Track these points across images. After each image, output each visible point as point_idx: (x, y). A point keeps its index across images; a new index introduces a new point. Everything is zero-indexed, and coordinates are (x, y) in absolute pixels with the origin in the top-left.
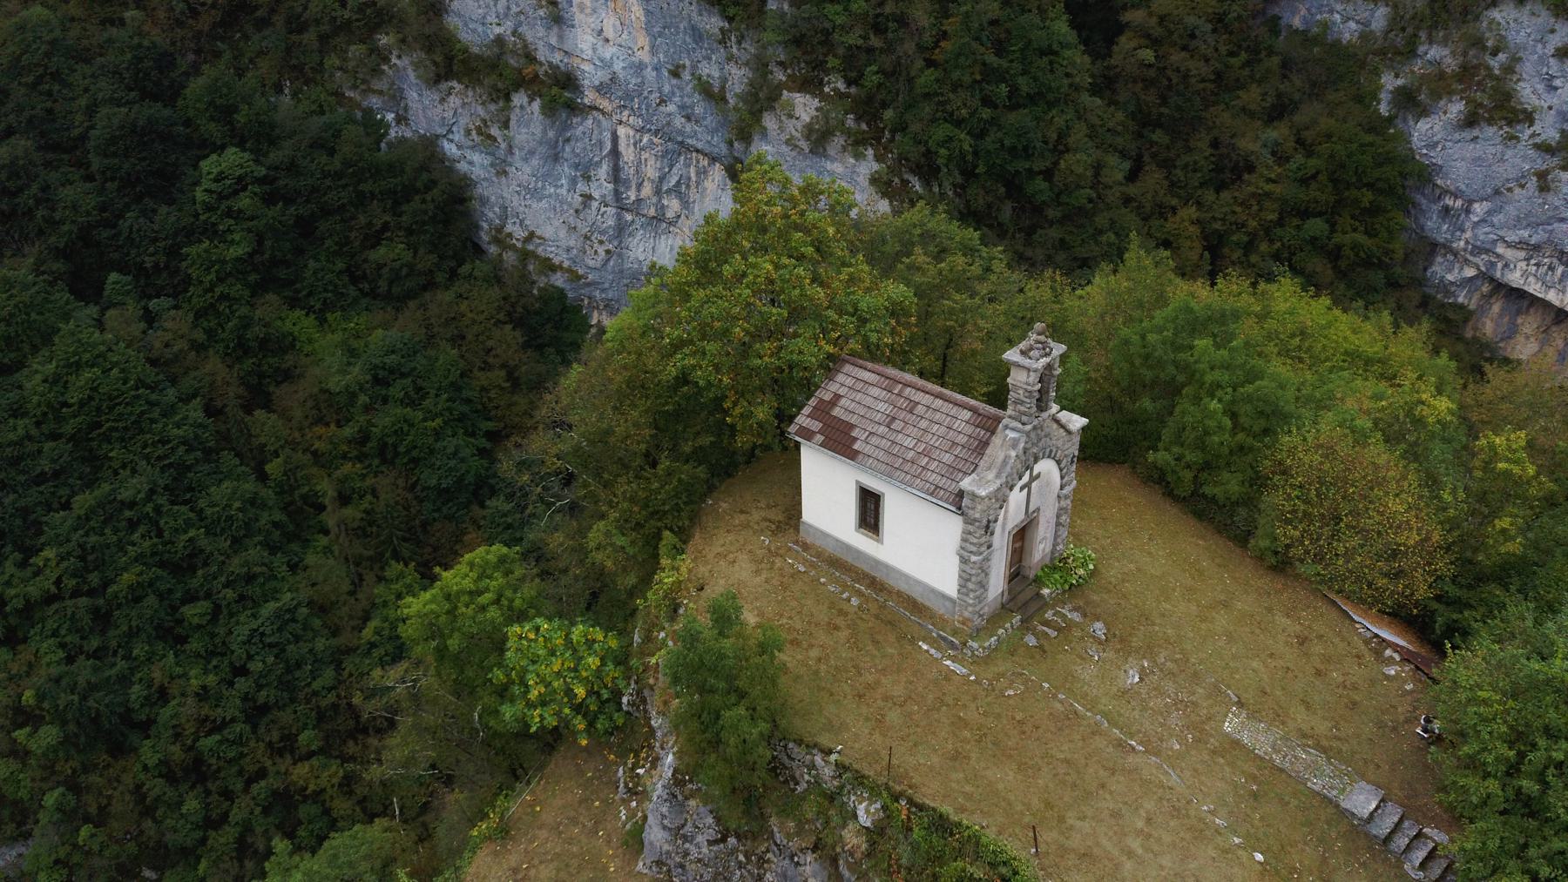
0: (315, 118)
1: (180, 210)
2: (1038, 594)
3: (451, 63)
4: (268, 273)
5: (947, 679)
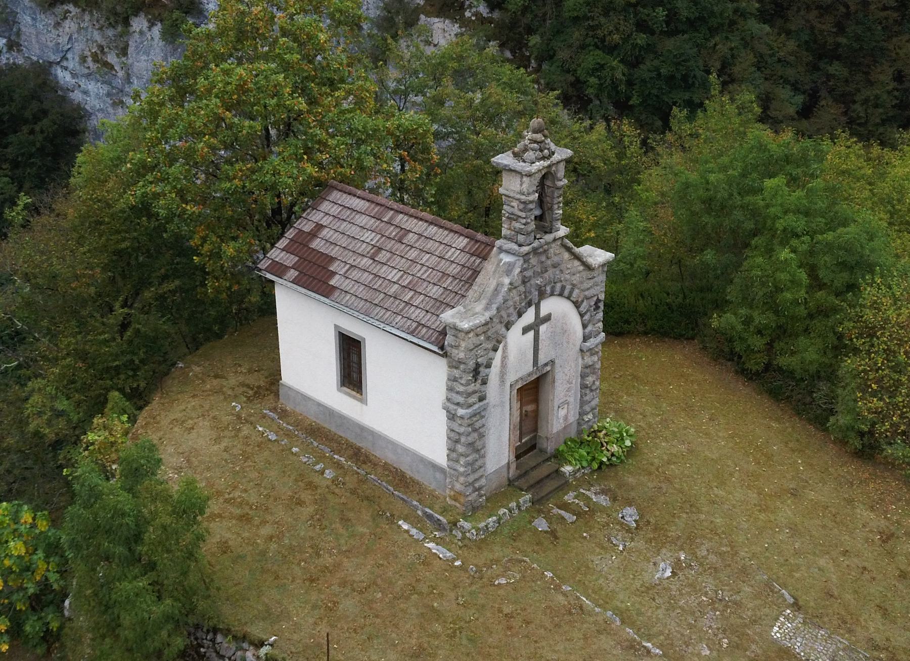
2: (557, 471)
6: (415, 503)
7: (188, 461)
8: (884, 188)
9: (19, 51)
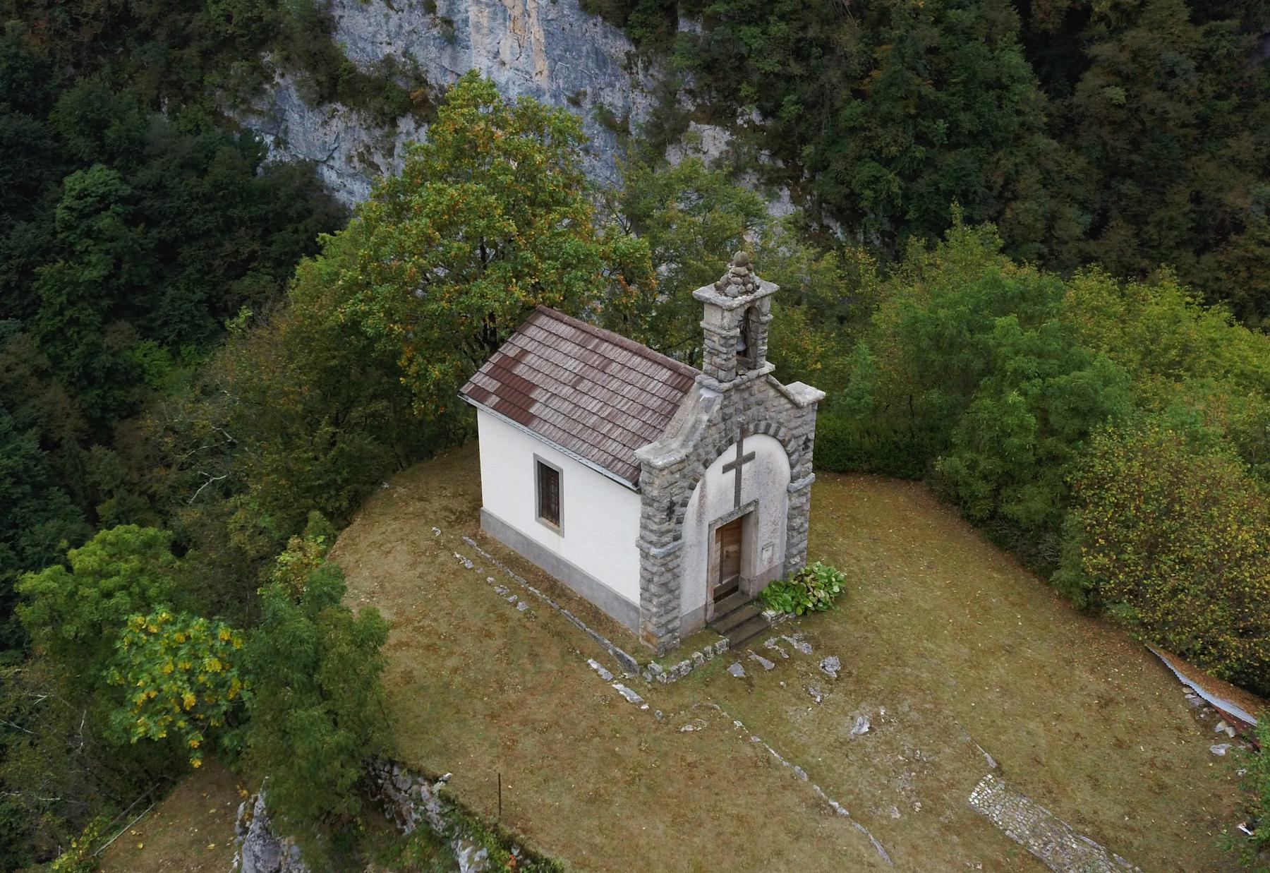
0: (189, 137)
1: (39, 227)
2: (759, 616)
3: (335, 84)
4: (123, 300)
5: (612, 705)
6: (606, 641)
7: (382, 586)
8: (1137, 328)
9: (286, 148)
